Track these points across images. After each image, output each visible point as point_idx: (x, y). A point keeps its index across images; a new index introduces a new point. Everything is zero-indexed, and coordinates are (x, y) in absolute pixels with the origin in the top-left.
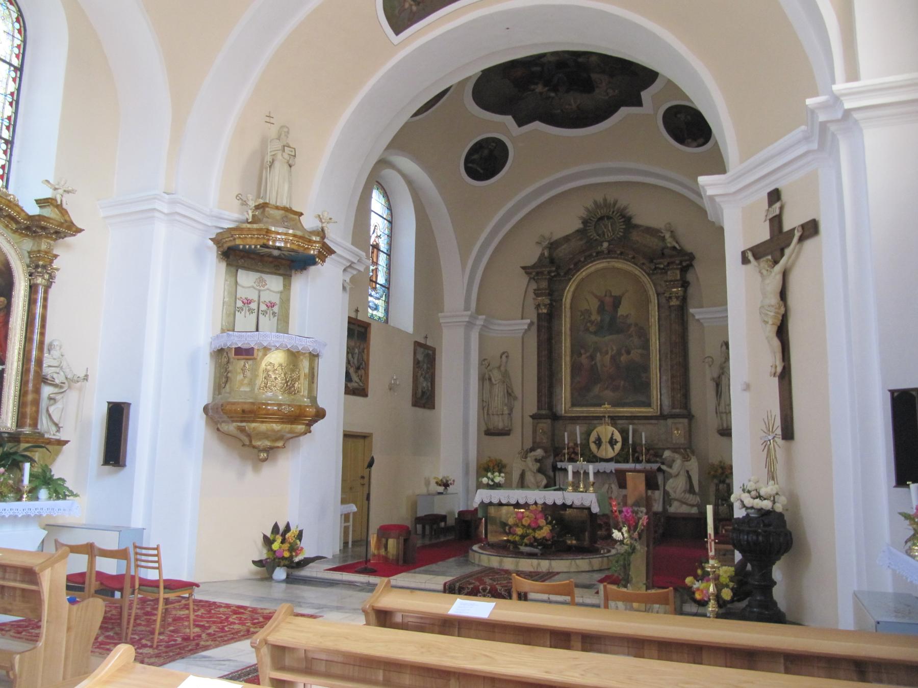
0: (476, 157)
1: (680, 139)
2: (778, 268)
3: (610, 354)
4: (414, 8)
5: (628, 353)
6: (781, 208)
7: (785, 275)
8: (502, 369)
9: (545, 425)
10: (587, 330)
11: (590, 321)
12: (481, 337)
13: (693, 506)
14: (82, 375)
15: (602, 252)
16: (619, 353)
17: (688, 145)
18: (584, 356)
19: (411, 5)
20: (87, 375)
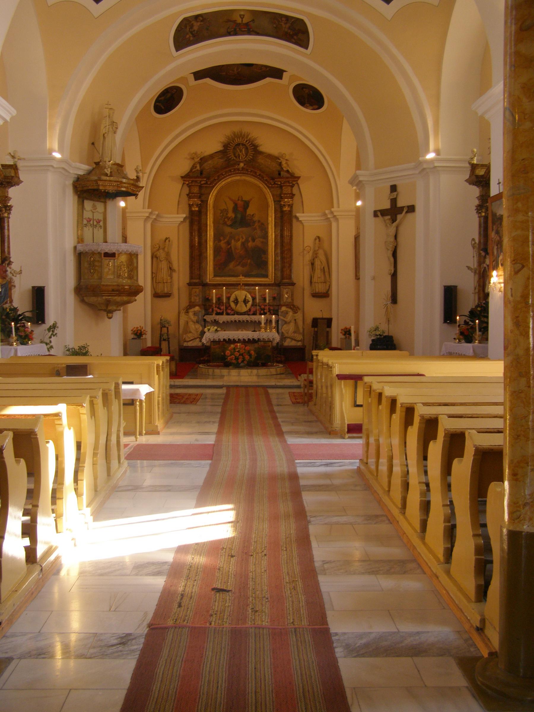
0: (162, 98)
1: (302, 103)
2: (395, 224)
3: (241, 240)
4: (191, 38)
5: (253, 240)
6: (397, 195)
7: (397, 227)
8: (166, 249)
9: (197, 290)
10: (225, 223)
11: (227, 217)
12: (152, 225)
13: (298, 341)
14: (18, 270)
15: (238, 169)
16: (247, 241)
17: (307, 107)
18: (222, 242)
19: (190, 37)
20: (21, 271)
